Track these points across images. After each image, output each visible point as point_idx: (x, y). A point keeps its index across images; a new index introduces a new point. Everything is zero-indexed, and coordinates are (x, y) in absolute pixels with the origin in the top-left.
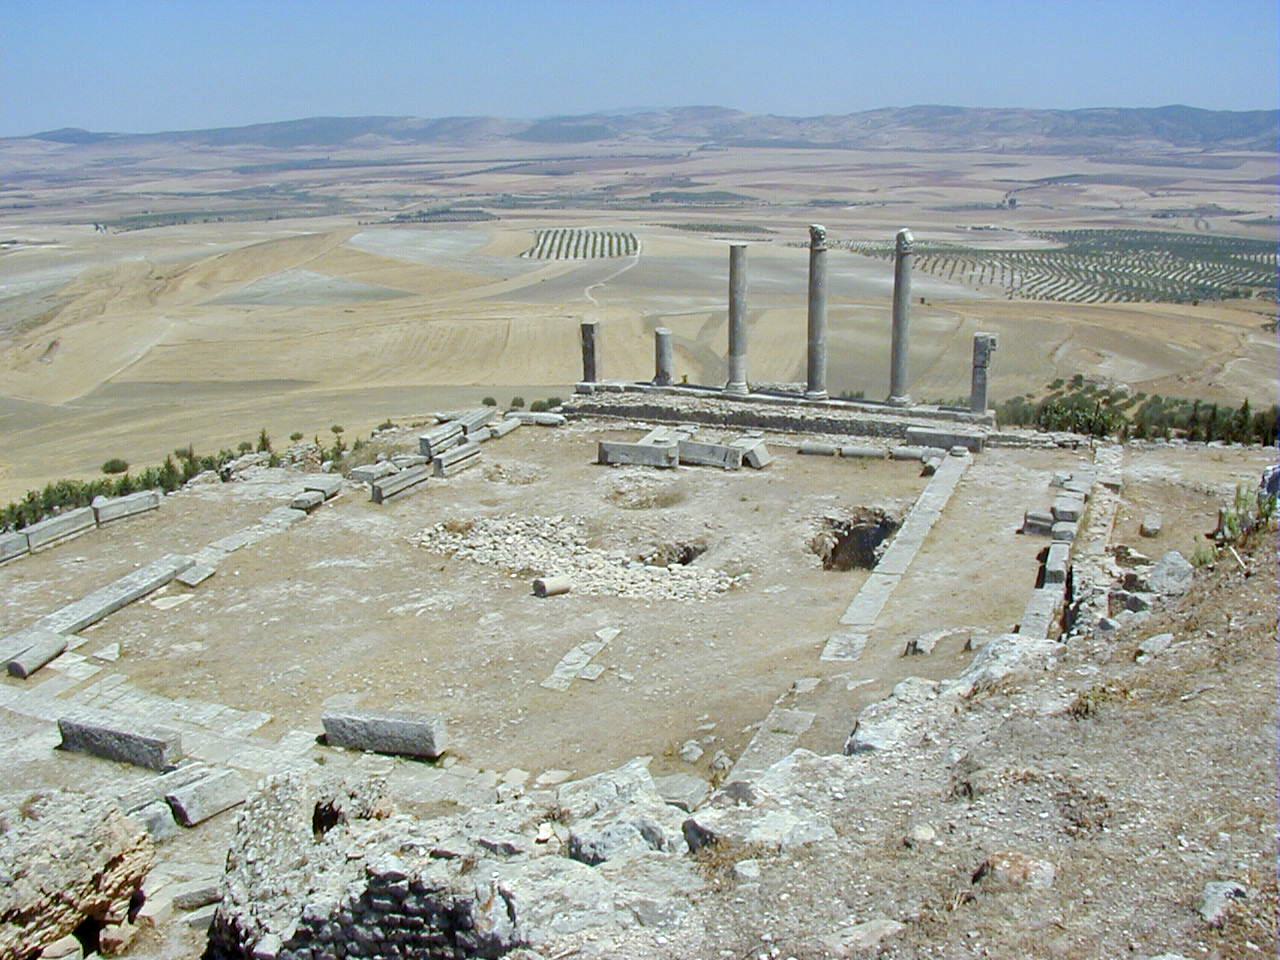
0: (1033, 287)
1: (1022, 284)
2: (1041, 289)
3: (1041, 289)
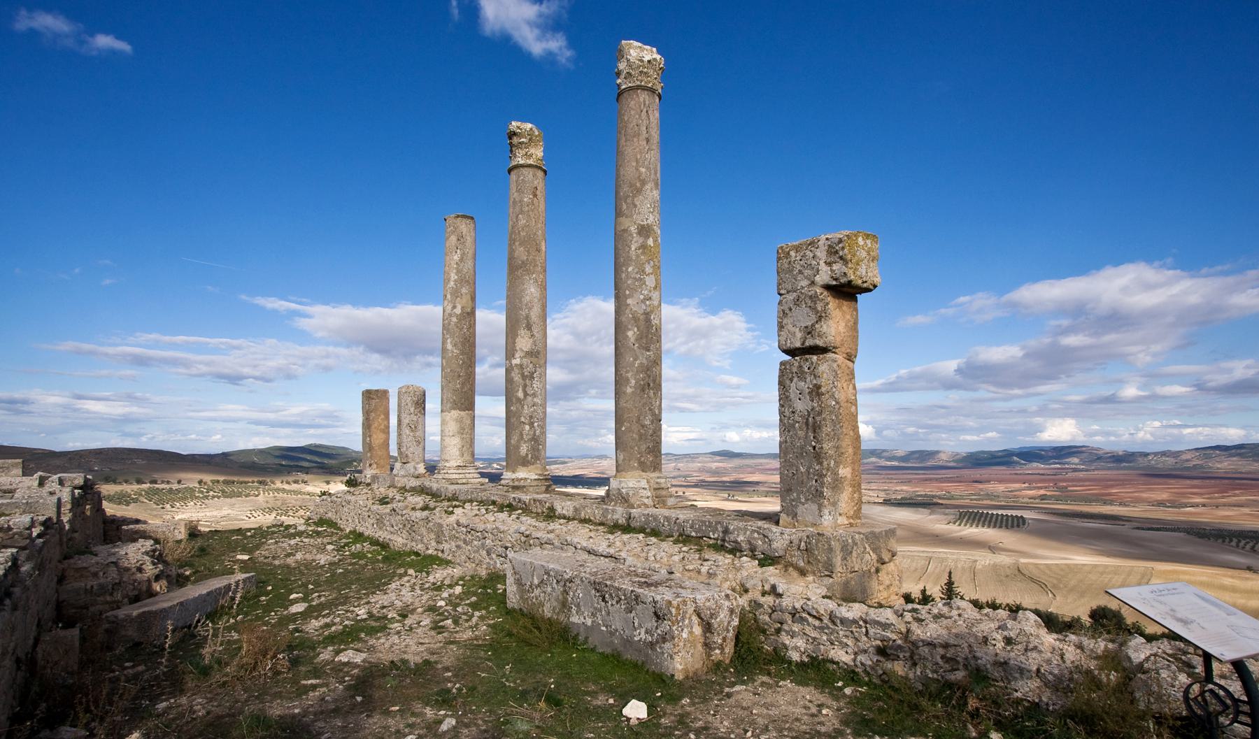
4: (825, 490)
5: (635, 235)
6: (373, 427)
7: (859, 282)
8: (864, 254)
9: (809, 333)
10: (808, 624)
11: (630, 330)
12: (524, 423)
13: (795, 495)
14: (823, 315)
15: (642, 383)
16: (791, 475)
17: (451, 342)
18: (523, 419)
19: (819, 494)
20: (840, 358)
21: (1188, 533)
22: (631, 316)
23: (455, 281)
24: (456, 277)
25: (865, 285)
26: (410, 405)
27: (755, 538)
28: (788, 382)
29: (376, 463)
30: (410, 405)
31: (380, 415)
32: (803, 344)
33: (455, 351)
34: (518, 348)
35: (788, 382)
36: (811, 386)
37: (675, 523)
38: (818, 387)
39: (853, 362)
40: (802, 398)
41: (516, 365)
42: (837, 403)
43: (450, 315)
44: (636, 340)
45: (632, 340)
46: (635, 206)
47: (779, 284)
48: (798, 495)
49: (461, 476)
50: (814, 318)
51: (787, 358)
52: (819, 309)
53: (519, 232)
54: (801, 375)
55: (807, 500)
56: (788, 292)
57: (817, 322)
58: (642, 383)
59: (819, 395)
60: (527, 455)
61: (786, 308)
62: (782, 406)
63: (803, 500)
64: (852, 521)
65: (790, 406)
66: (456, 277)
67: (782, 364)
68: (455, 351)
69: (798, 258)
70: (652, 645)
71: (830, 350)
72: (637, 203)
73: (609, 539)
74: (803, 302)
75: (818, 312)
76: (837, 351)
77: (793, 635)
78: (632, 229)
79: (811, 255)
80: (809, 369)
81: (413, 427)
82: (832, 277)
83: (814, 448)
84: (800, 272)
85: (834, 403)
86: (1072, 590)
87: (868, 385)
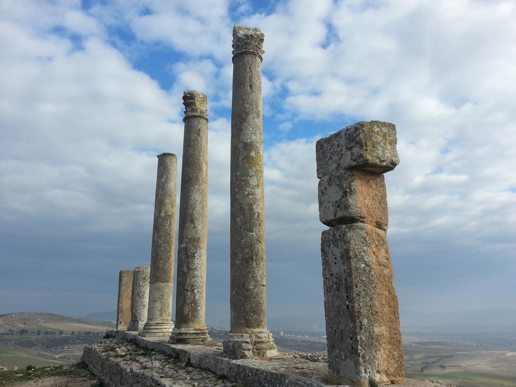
4: (360, 347)
5: (241, 150)
6: (124, 296)
7: (377, 161)
8: (380, 138)
9: (338, 206)
11: (238, 217)
13: (337, 351)
14: (348, 190)
15: (247, 256)
16: (333, 332)
19: (354, 352)
20: (369, 227)
22: (238, 207)
25: (384, 164)
28: (327, 248)
29: (124, 321)
31: (129, 288)
32: (335, 216)
34: (184, 236)
35: (327, 248)
36: (342, 251)
37: (256, 374)
38: (348, 251)
39: (384, 230)
40: (337, 262)
42: (367, 265)
48: (340, 351)
50: (340, 194)
51: (327, 228)
52: (345, 186)
54: (335, 242)
55: (346, 357)
56: (324, 176)
57: (343, 197)
58: (247, 256)
59: (349, 258)
62: (324, 270)
63: (343, 357)
64: (393, 378)
67: (324, 233)
69: (329, 148)
71: (357, 220)
73: (383, 385)
74: (333, 182)
75: (343, 188)
76: (365, 220)
79: (337, 143)
80: (340, 237)
82: (352, 159)
84: (331, 158)
85: (364, 265)
87: (142, 207)
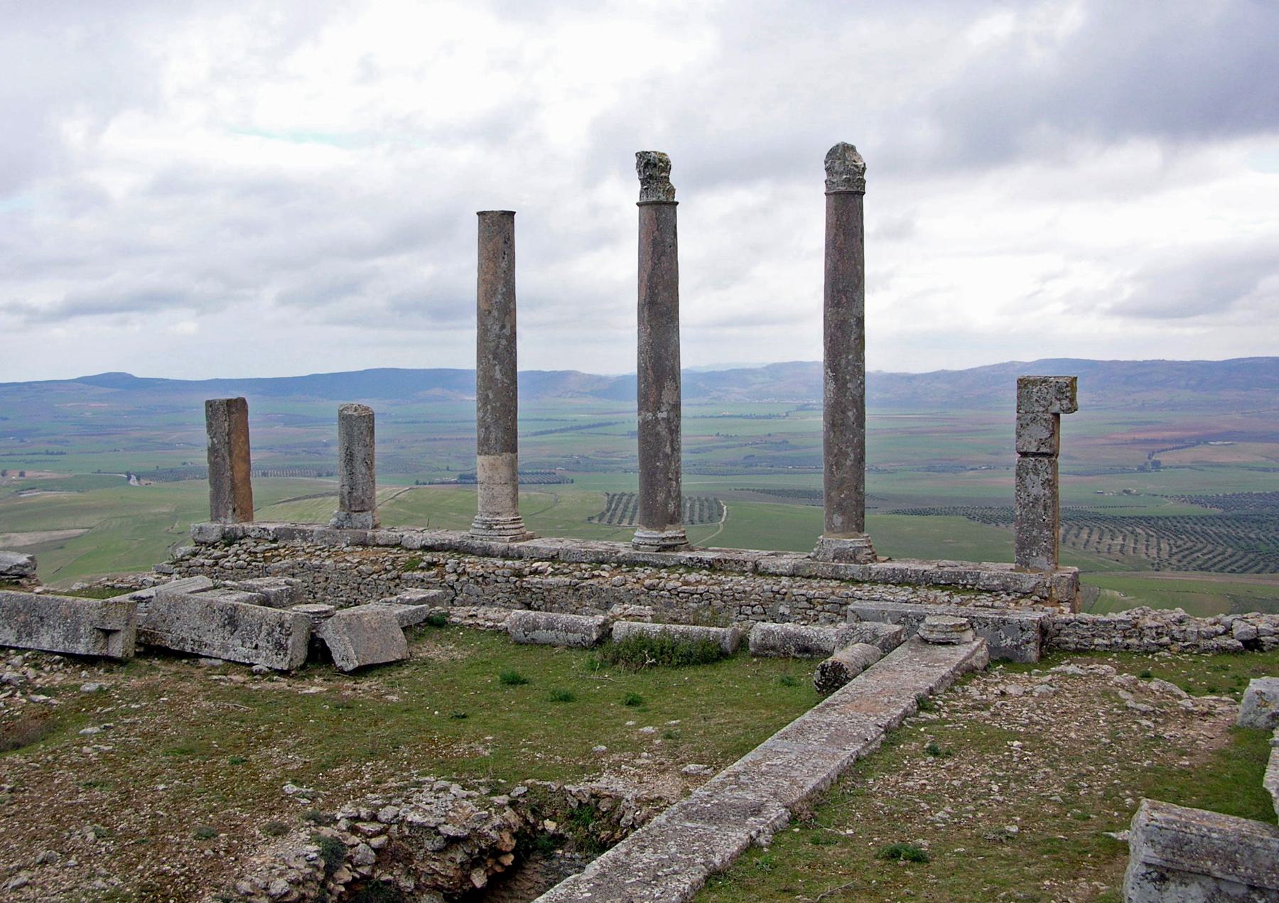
0: (1184, 557)
1: (1171, 556)
2: (1194, 560)
3: (1194, 560)
10: (1079, 628)
12: (671, 479)
17: (501, 370)
18: (670, 476)
21: (971, 518)
23: (503, 294)
24: (504, 290)
26: (365, 433)
27: (1007, 582)
30: (365, 433)
32: (1038, 450)
33: (505, 381)
41: (663, 419)
43: (499, 337)
44: (856, 419)
45: (852, 419)
46: (854, 301)
47: (1018, 406)
49: (518, 531)
53: (663, 275)
60: (674, 512)
61: (1024, 423)
65: (1025, 492)
66: (504, 290)
68: (505, 381)
70: (1017, 647)
72: (856, 298)
77: (1068, 635)
78: (852, 321)
81: (369, 462)
83: (1044, 520)
86: (1025, 595)
